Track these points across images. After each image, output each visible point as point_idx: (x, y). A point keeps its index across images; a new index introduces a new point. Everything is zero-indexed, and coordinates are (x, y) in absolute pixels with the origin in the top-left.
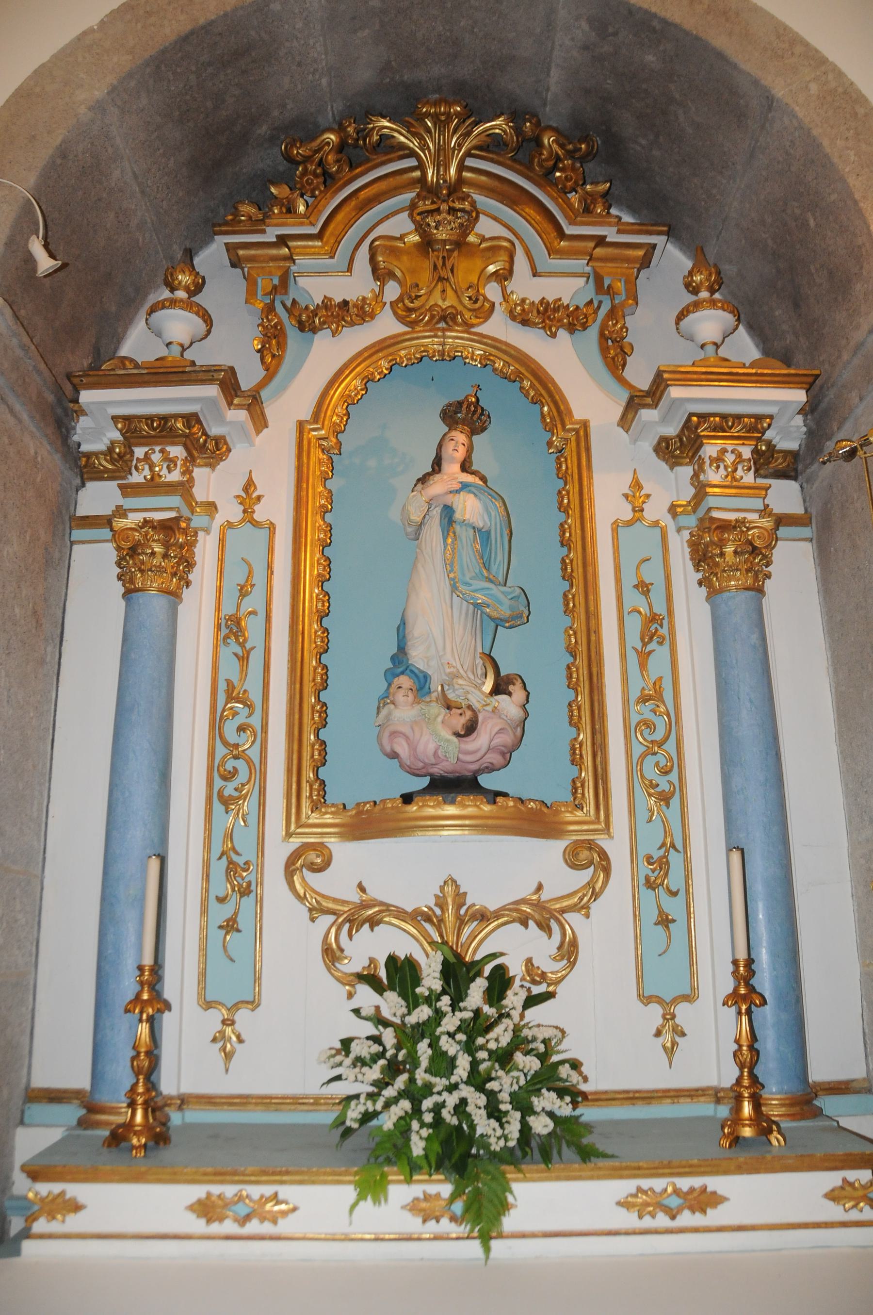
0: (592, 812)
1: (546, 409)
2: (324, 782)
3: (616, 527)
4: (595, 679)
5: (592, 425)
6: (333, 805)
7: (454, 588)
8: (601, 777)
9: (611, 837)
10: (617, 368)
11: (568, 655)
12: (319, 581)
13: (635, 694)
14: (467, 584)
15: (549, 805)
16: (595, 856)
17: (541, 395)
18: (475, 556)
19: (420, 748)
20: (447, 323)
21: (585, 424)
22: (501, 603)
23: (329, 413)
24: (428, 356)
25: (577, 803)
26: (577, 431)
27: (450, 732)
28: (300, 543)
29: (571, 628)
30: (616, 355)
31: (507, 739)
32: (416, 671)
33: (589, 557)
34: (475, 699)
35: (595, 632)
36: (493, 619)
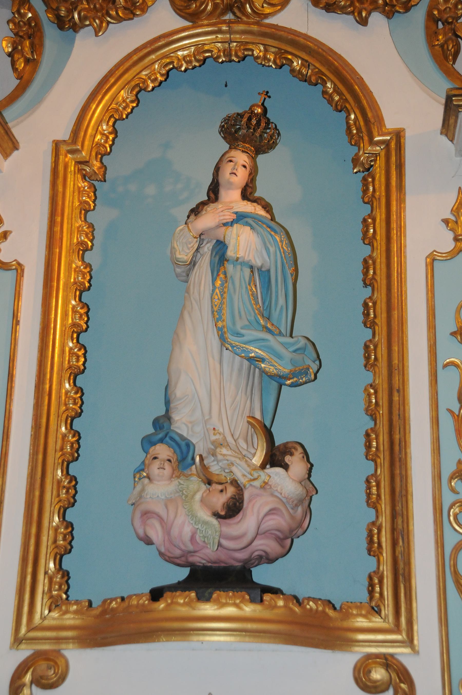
0: (391, 618)
1: (353, 116)
2: (68, 573)
3: (432, 260)
4: (397, 448)
5: (408, 134)
6: (77, 602)
7: (223, 339)
8: (402, 574)
9: (415, 652)
10: (446, 58)
11: (368, 418)
12: (73, 332)
13: (449, 466)
14: (238, 335)
15: (338, 607)
16: (394, 675)
17: (346, 100)
18: (250, 302)
19: (175, 532)
20: (234, 14)
21: (399, 135)
22: (279, 357)
23: (90, 131)
24: (211, 56)
25: (373, 604)
26: (387, 143)
27: (209, 513)
28: (51, 287)
29: (371, 385)
30: (446, 42)
31: (279, 522)
32: (177, 438)
33: (395, 301)
34: (240, 473)
35: (398, 391)
36: (272, 377)
